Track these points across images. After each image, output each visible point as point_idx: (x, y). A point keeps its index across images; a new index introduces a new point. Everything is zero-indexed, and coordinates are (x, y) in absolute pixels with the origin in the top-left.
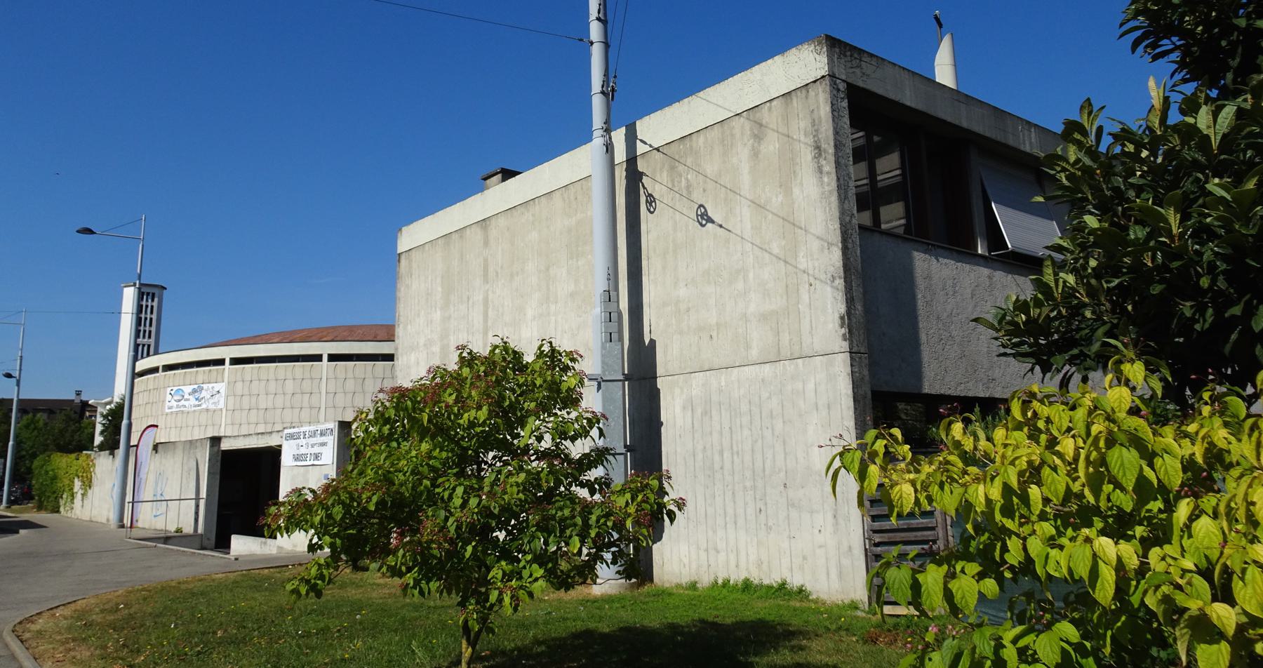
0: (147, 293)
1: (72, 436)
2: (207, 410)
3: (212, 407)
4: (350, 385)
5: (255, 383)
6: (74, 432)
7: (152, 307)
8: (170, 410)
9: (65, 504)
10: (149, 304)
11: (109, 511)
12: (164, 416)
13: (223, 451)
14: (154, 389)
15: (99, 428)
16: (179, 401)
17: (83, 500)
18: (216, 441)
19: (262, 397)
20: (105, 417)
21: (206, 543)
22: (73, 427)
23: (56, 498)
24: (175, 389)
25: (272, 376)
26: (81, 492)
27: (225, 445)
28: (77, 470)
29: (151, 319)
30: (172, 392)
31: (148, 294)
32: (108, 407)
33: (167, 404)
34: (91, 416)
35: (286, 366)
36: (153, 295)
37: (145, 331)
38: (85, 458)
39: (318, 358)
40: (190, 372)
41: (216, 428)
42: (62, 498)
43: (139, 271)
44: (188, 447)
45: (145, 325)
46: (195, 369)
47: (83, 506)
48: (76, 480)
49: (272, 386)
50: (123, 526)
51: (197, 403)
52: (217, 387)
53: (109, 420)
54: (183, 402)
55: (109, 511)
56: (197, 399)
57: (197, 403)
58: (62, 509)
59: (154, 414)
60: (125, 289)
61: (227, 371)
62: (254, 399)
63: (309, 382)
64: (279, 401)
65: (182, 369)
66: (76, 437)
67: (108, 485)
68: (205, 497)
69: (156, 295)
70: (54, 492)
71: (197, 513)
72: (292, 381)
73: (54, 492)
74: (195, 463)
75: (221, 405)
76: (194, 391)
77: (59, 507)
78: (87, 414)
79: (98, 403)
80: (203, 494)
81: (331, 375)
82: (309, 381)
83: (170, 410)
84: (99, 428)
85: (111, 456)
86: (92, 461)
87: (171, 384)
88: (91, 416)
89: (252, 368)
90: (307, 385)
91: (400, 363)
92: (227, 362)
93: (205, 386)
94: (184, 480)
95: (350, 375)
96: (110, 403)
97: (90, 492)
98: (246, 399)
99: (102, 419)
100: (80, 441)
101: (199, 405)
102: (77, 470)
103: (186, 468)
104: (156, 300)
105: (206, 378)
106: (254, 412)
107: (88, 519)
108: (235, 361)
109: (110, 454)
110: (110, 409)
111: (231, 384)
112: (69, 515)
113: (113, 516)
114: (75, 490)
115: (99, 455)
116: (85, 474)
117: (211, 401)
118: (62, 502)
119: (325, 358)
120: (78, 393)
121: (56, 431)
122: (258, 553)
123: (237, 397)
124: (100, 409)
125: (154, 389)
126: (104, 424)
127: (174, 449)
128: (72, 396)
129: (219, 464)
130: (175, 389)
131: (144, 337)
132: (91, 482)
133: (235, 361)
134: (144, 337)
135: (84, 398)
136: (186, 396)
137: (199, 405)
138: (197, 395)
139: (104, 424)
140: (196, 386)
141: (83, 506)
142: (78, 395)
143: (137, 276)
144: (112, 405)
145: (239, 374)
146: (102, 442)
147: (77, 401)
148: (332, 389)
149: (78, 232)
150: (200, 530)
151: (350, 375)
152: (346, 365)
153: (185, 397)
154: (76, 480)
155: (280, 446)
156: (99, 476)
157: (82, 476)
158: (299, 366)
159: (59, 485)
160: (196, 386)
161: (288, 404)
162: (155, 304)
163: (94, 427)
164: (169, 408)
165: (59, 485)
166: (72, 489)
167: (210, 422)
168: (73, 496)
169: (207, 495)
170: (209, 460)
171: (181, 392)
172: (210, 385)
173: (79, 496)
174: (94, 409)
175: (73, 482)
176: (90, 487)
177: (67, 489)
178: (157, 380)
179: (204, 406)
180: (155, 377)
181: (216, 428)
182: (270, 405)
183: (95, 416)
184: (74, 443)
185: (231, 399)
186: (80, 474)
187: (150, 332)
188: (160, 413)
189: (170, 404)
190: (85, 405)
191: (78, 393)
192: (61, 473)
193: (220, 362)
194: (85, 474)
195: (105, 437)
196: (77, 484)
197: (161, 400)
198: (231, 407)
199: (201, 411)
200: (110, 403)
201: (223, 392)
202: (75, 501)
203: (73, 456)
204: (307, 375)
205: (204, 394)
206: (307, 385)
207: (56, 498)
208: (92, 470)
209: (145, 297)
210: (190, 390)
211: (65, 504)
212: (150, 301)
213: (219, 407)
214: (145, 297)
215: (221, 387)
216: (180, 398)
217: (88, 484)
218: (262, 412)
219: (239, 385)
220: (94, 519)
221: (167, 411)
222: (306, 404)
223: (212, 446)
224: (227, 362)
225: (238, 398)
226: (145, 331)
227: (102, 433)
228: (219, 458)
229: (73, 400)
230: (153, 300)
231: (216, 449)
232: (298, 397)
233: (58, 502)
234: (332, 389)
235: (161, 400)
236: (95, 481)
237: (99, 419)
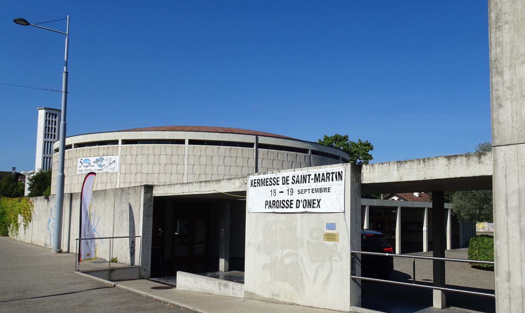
0: (52, 113)
1: (13, 190)
2: (107, 173)
3: (110, 171)
4: (203, 160)
5: (140, 157)
6: (13, 187)
7: (55, 121)
8: (81, 173)
9: (12, 231)
10: (54, 120)
11: (46, 239)
12: (77, 176)
13: (156, 198)
14: (69, 159)
15: (27, 186)
16: (87, 166)
17: (25, 229)
18: (149, 188)
19: (145, 166)
20: (31, 180)
21: (143, 273)
22: (12, 185)
23: (5, 226)
24: (84, 159)
25: (151, 152)
26: (23, 224)
27: (158, 192)
28: (20, 209)
29: (55, 128)
30: (82, 161)
31: (53, 114)
32: (32, 175)
33: (79, 168)
34: (21, 181)
35: (160, 146)
36: (56, 115)
37: (52, 135)
38: (25, 201)
39: (182, 142)
40: (94, 148)
41: (114, 184)
42: (9, 226)
43: (65, 59)
44: (119, 193)
45: (51, 131)
46: (97, 147)
47: (25, 233)
48: (19, 215)
49: (151, 159)
50: (60, 252)
51: (100, 168)
52: (113, 158)
53: (33, 182)
54: (89, 168)
55: (46, 239)
56: (99, 166)
57: (100, 168)
58: (10, 234)
59: (69, 175)
60: (39, 111)
61: (120, 148)
62: (139, 167)
63: (176, 157)
64: (156, 169)
65: (88, 146)
66: (15, 190)
67: (45, 220)
68: (141, 234)
69: (57, 115)
70: (4, 223)
71: (64, 223)
72: (165, 156)
73: (4, 223)
74: (128, 207)
75: (117, 170)
76: (98, 161)
77: (8, 232)
78: (19, 179)
79: (26, 173)
80: (139, 231)
81: (191, 153)
82: (176, 157)
83: (81, 173)
84: (27, 186)
85: (47, 200)
86: (31, 203)
87: (81, 156)
88: (21, 181)
89: (137, 147)
90: (175, 159)
91: (507, 77)
92: (120, 142)
93: (105, 157)
94: (117, 220)
95: (203, 153)
96: (33, 173)
97: (30, 224)
98: (133, 167)
99: (29, 181)
100: (17, 192)
101: (101, 170)
102: (20, 209)
103: (118, 210)
104: (57, 117)
105: (105, 152)
106: (139, 176)
107: (30, 242)
108: (125, 142)
109: (46, 198)
110: (34, 176)
111: (123, 157)
112: (15, 238)
113: (52, 244)
114: (19, 222)
115: (37, 199)
116: (26, 212)
117: (109, 167)
118: (10, 229)
119: (187, 142)
120: (14, 169)
121: (3, 186)
122: (215, 293)
123: (127, 165)
124: (27, 177)
125: (69, 159)
126: (30, 184)
127: (105, 195)
128: (10, 170)
129: (152, 208)
130: (84, 159)
131: (51, 138)
132: (31, 217)
133: (125, 142)
134: (51, 138)
135: (17, 171)
136: (92, 164)
137: (101, 170)
138: (99, 163)
139: (30, 184)
140: (98, 158)
141: (25, 233)
142: (14, 169)
143: (65, 63)
144: (35, 174)
145: (128, 150)
146: (29, 194)
147: (14, 172)
148: (191, 162)
149: (15, 21)
150: (138, 261)
151: (203, 153)
152: (200, 147)
153: (91, 164)
154: (19, 215)
155: (244, 193)
156: (37, 213)
157: (24, 213)
158: (216, 147)
159: (7, 218)
160: (98, 158)
161: (162, 171)
162: (57, 120)
163: (24, 186)
164: (80, 171)
165: (7, 218)
166: (17, 221)
167: (109, 181)
168: (17, 226)
169: (144, 233)
170: (144, 204)
171: (88, 161)
172: (109, 157)
173: (21, 227)
174: (23, 176)
175: (17, 217)
176: (30, 221)
177: (13, 221)
178: (70, 153)
179: (105, 170)
180: (69, 151)
181: (114, 184)
182: (150, 171)
183: (24, 181)
184: (14, 193)
185: (123, 167)
186: (22, 212)
187: (55, 135)
188: (74, 174)
189: (81, 169)
190: (18, 175)
191: (14, 169)
192: (8, 210)
193: (116, 142)
194: (26, 212)
195: (31, 191)
196: (20, 218)
197: (74, 166)
198: (123, 171)
199: (102, 174)
200: (33, 173)
201: (117, 161)
202: (19, 229)
203: (16, 199)
204: (175, 153)
205: (104, 162)
206: (175, 159)
207: (5, 226)
208: (31, 209)
209: (51, 116)
210: (95, 160)
211: (12, 231)
212: (54, 118)
213: (115, 171)
214: (51, 116)
215: (117, 158)
216: (87, 165)
217: (28, 218)
218: (145, 175)
219: (129, 157)
220: (34, 243)
221: (78, 173)
222: (174, 171)
223: (146, 193)
224: (120, 142)
225: (128, 166)
226: (52, 135)
227: (29, 189)
228: (152, 203)
229: (11, 172)
230: (56, 118)
231: (149, 195)
232: (169, 166)
233: (7, 229)
234: (191, 162)
235: (74, 166)
236: (33, 216)
237: (27, 181)
